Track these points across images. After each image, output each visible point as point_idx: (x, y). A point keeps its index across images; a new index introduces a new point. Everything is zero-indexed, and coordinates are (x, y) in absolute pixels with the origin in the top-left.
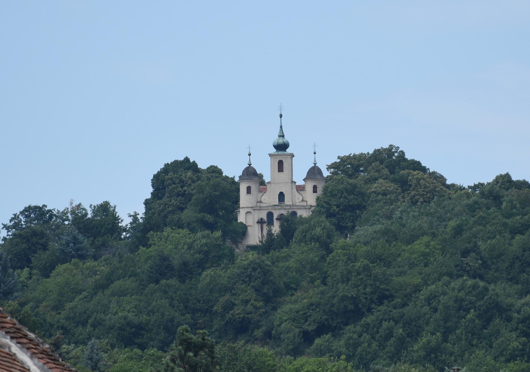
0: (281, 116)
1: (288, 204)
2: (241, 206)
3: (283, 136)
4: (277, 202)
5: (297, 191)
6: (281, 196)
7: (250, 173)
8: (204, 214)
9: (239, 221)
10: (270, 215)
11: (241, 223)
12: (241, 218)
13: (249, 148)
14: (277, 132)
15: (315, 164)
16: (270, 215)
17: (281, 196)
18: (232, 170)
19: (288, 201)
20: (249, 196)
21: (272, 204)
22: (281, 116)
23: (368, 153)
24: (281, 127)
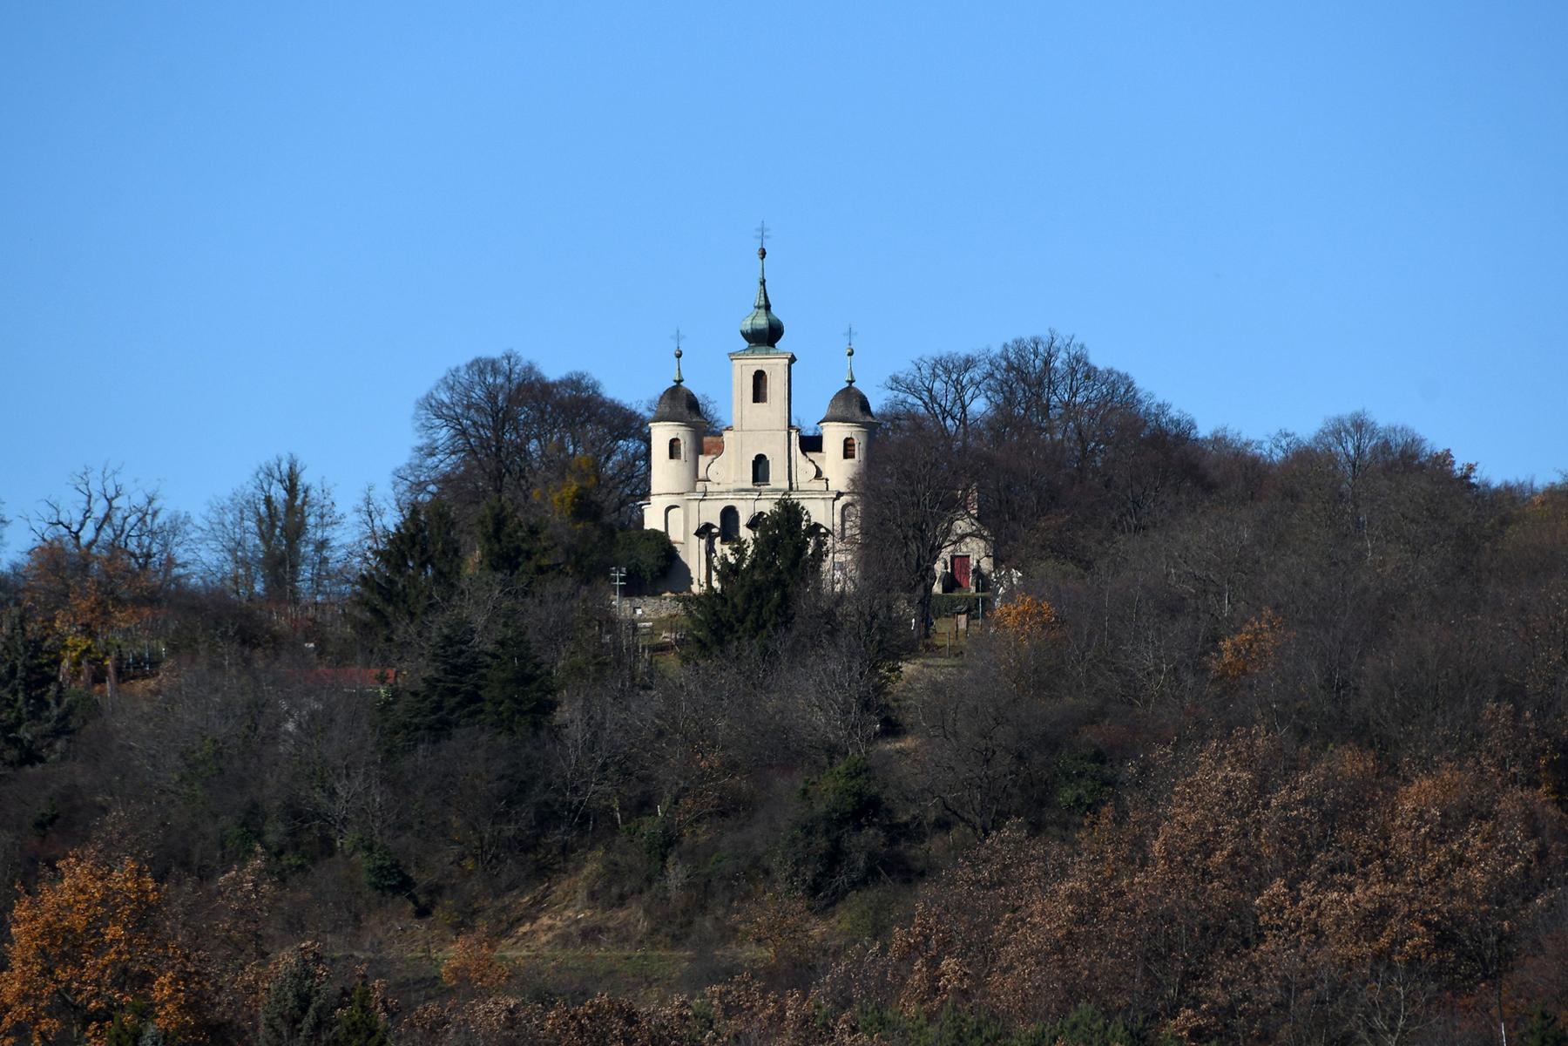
0: (763, 254)
1: (779, 486)
2: (653, 491)
3: (767, 307)
4: (748, 483)
5: (804, 450)
6: (760, 467)
7: (683, 405)
8: (36, 1033)
9: (647, 527)
10: (729, 514)
11: (655, 532)
12: (653, 519)
13: (678, 337)
14: (756, 297)
15: (851, 382)
16: (729, 514)
17: (760, 467)
18: (630, 385)
19: (777, 478)
20: (674, 462)
21: (732, 487)
22: (763, 254)
23: (285, 519)
24: (763, 283)
